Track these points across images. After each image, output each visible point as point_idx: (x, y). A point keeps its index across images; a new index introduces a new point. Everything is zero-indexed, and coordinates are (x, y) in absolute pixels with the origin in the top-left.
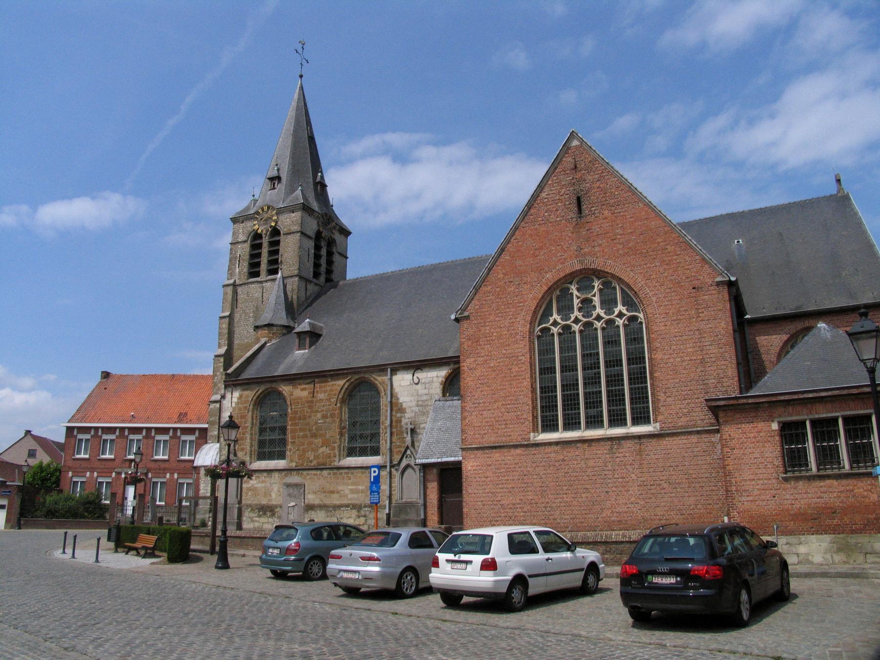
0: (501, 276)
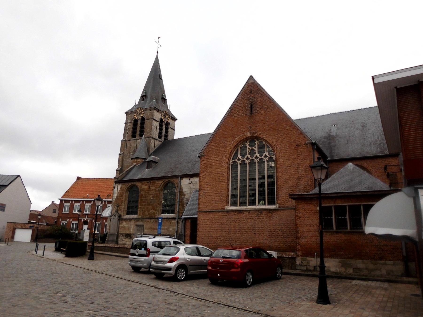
0: (218, 138)
